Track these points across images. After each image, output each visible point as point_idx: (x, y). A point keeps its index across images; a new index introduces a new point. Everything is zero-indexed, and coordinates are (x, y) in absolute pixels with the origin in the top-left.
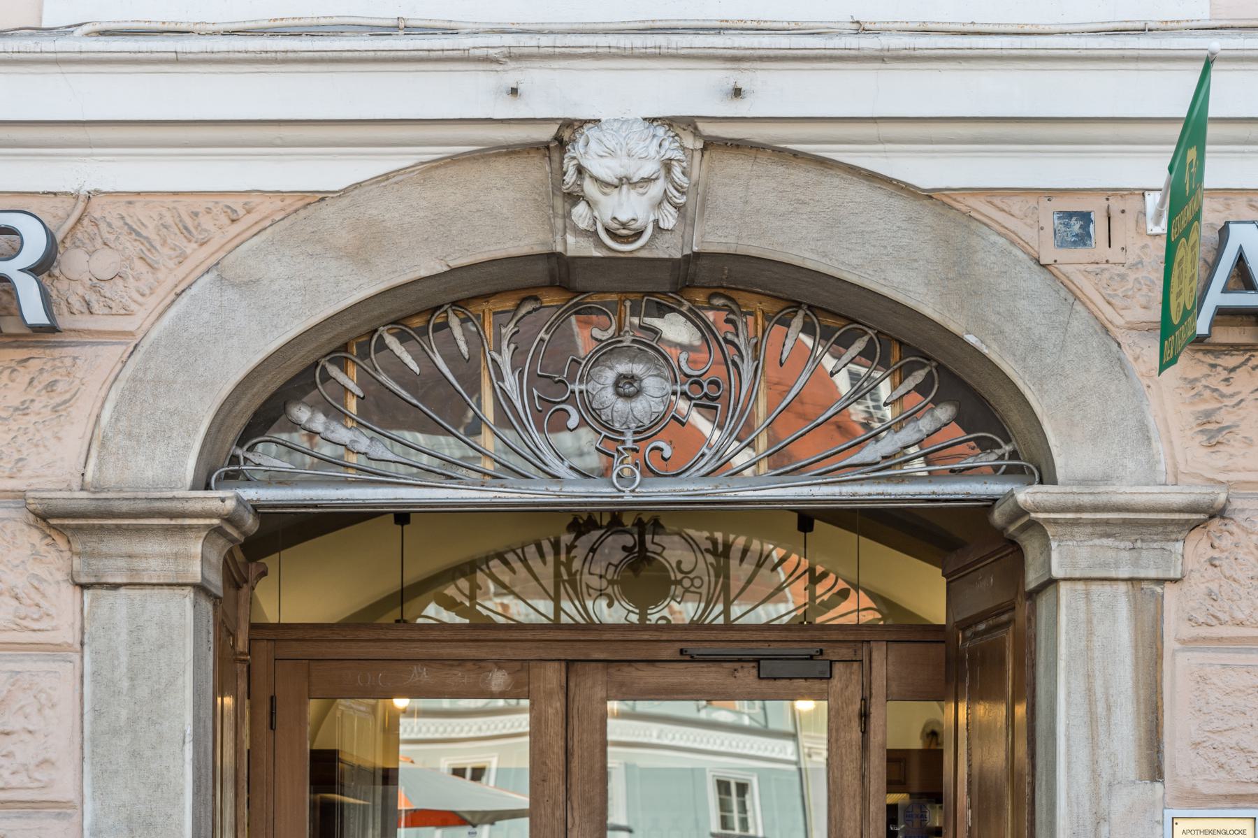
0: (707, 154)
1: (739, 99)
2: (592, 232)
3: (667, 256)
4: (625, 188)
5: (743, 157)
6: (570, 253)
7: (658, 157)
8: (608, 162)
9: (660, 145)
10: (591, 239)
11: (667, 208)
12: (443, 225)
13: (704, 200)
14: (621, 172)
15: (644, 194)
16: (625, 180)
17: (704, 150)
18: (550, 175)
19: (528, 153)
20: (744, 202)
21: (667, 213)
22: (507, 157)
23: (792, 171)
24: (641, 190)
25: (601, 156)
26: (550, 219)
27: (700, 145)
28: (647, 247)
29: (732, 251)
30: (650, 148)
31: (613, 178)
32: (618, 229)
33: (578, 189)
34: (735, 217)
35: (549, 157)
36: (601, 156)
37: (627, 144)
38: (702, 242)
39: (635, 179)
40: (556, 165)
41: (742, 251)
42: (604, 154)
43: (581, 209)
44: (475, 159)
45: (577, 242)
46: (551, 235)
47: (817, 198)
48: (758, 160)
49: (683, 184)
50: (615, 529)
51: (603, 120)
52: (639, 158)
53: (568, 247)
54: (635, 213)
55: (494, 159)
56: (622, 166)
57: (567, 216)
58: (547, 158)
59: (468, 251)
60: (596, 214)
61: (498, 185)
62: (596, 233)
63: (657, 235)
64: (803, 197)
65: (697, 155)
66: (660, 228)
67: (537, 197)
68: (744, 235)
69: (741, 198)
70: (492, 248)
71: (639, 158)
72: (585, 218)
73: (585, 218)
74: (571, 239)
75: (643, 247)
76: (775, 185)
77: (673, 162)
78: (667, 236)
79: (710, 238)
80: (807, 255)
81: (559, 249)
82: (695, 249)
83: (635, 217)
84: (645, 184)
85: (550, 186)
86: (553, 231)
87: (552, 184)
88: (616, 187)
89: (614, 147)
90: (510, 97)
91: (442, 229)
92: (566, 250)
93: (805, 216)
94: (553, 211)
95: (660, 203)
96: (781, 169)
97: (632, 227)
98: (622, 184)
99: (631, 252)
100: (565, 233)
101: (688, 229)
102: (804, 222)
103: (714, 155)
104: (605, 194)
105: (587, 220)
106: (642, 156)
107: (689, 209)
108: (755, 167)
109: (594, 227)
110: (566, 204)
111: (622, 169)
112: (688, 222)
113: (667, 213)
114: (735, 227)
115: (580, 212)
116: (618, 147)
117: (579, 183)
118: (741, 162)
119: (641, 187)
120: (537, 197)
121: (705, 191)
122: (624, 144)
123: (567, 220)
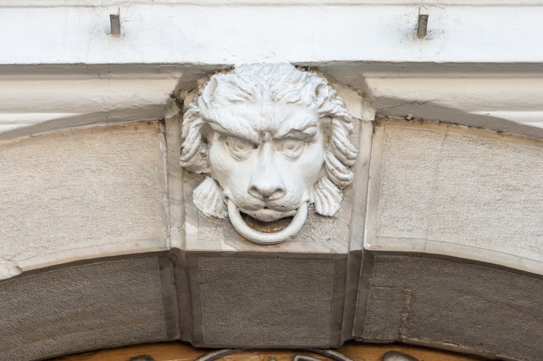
0: (380, 131)
1: (424, 41)
2: (222, 220)
3: (327, 251)
4: (267, 147)
5: (429, 134)
6: (190, 247)
7: (313, 106)
8: (243, 108)
9: (317, 92)
10: (220, 229)
11: (327, 186)
12: (13, 216)
13: (378, 186)
14: (264, 123)
15: (295, 158)
16: (267, 135)
17: (376, 123)
18: (165, 154)
19: (136, 128)
20: (433, 188)
21: (327, 193)
22: (106, 134)
23: (497, 151)
24: (291, 153)
25: (234, 102)
26: (163, 208)
27: (370, 116)
28: (299, 239)
29: (418, 249)
30: (303, 93)
31: (251, 129)
32: (258, 207)
33: (201, 162)
34: (422, 206)
35: (165, 134)
36: (234, 102)
37: (271, 86)
38: (377, 237)
39: (282, 132)
40: (173, 140)
41: (431, 249)
42: (238, 98)
43: (207, 185)
44: (62, 135)
45: (199, 233)
46: (163, 229)
47: (534, 183)
48: (449, 138)
49: (348, 151)
50: (347, 183)
51: (237, 64)
52: (288, 103)
53: (188, 239)
54: (282, 182)
55: (90, 136)
56: (263, 115)
57: (188, 199)
58: (162, 135)
59: (47, 248)
60: (228, 192)
61: (94, 167)
62: (228, 220)
63: (313, 224)
64: (514, 183)
65: (367, 129)
66: (317, 214)
67: (146, 181)
68: (435, 228)
69: (428, 183)
70: (80, 245)
71: (288, 103)
72: (212, 199)
73: (212, 199)
74: (191, 229)
75: (293, 238)
76: (474, 168)
77: (335, 121)
78: (328, 225)
79: (387, 232)
80: (524, 254)
81: (176, 243)
82: (368, 246)
83: (282, 186)
84: (296, 144)
85: (165, 167)
86: (167, 224)
87: (168, 163)
88: (256, 146)
89: (252, 89)
90: (110, 37)
91: (12, 220)
92: (184, 244)
93: (518, 206)
94: (168, 198)
95: (317, 182)
96: (483, 149)
97: (278, 202)
98: (264, 142)
99: (276, 244)
100: (183, 220)
101: (357, 219)
102: (518, 212)
103: (389, 131)
104: (239, 158)
105: (215, 202)
106: (292, 100)
107: (358, 194)
108: (446, 146)
109: (225, 214)
110: (185, 185)
111: (264, 119)
112: (357, 209)
113: (327, 193)
114: (422, 219)
115: (204, 192)
116: (258, 90)
117: (203, 151)
118: (427, 139)
119: (291, 148)
120: (146, 181)
121: (378, 175)
122: (266, 87)
123: (187, 205)
